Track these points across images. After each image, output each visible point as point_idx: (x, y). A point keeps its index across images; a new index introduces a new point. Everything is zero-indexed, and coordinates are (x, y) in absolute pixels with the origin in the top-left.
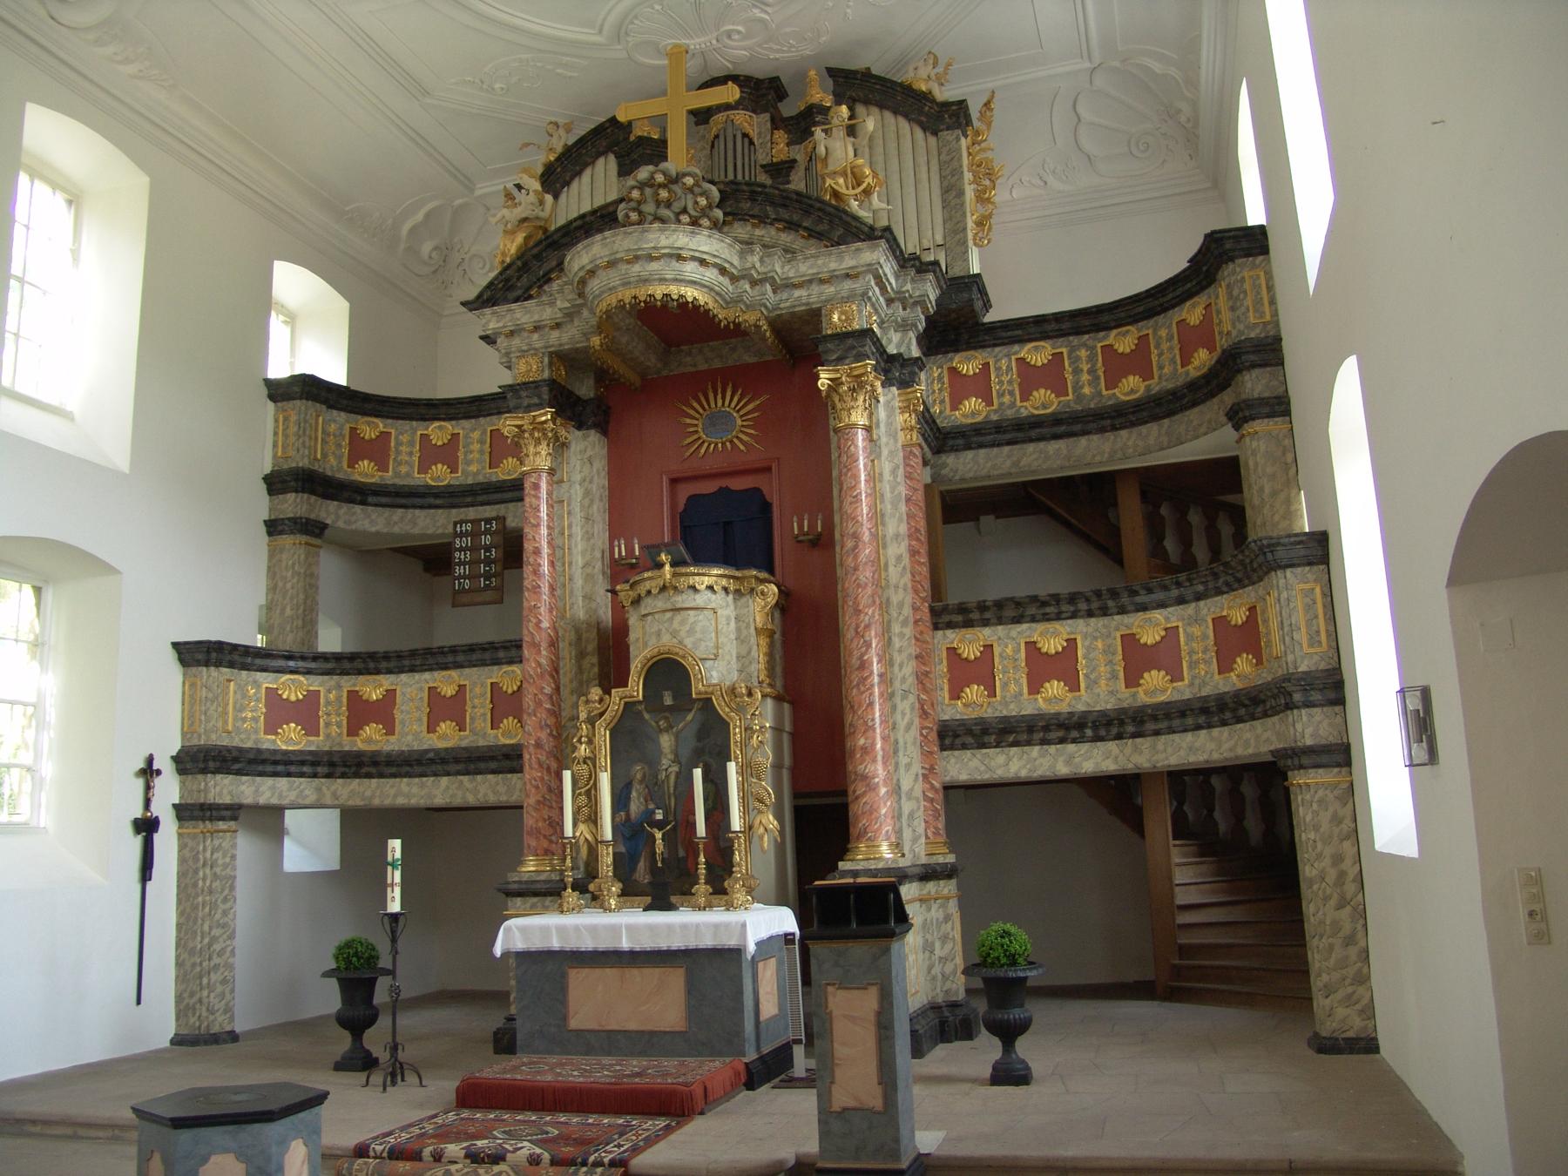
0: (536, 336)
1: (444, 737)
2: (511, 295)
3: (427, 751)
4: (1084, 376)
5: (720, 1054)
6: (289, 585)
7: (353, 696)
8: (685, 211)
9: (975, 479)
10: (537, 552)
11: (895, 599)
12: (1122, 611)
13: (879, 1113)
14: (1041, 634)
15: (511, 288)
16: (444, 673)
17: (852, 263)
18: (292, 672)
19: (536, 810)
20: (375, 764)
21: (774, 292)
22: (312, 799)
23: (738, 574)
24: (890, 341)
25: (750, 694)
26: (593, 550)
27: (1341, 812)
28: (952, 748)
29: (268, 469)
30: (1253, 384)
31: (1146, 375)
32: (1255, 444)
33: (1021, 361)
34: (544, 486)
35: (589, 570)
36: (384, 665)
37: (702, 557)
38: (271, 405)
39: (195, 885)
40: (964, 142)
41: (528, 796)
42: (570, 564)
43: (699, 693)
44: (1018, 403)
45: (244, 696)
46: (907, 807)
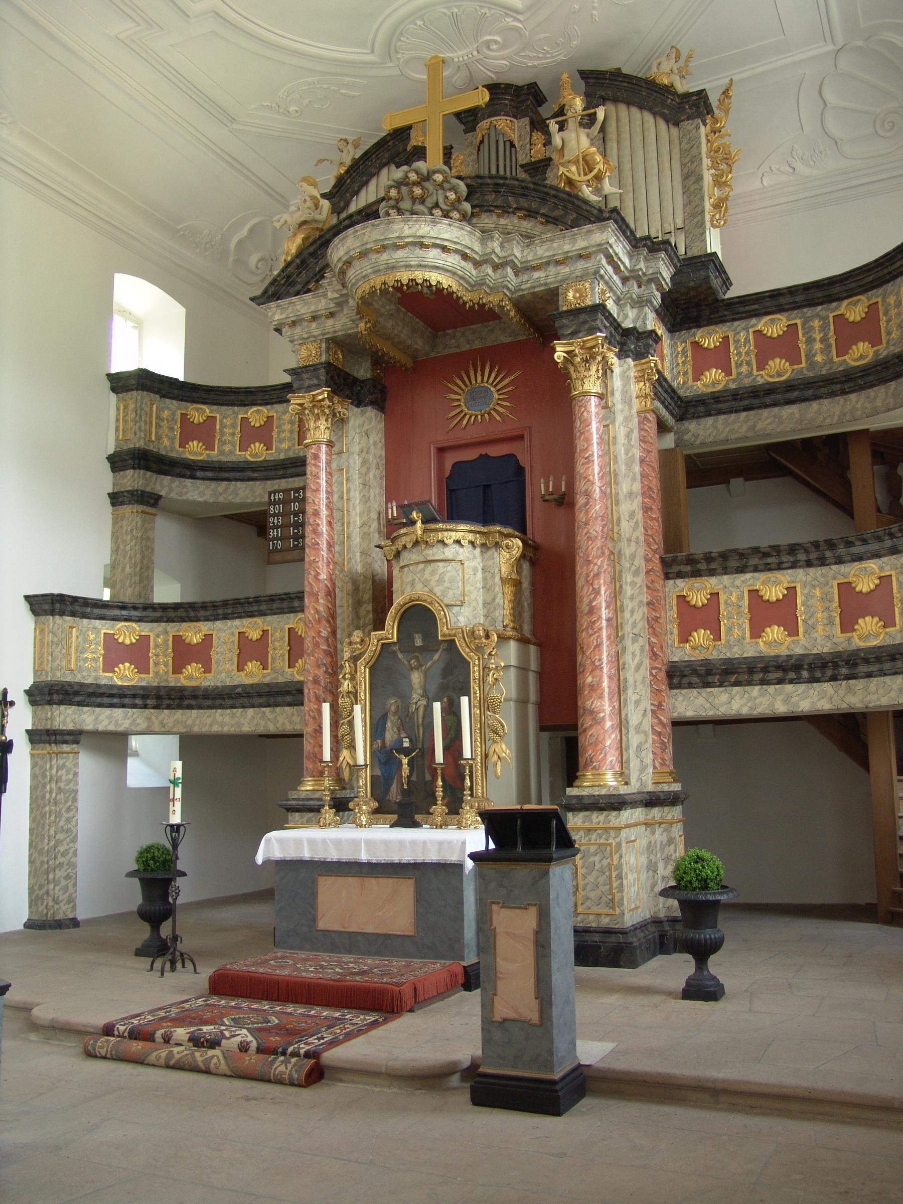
0: (314, 325)
1: (250, 674)
2: (293, 290)
3: (236, 687)
4: (817, 344)
5: (443, 957)
6: (128, 548)
7: (178, 640)
8: (437, 205)
9: (714, 443)
10: (316, 513)
11: (627, 551)
12: (839, 561)
13: (535, 1025)
14: (763, 583)
15: (292, 284)
16: (250, 620)
18: (126, 620)
19: (312, 737)
20: (195, 697)
21: (516, 275)
22: (143, 726)
23: (483, 529)
24: (626, 316)
25: (487, 636)
26: (369, 512)
28: (679, 686)
29: (111, 451)
31: (875, 341)
33: (758, 333)
34: (323, 457)
35: (366, 529)
36: (202, 613)
37: (455, 513)
38: (113, 397)
39: (43, 797)
40: (703, 130)
41: (306, 725)
42: (348, 524)
43: (444, 635)
44: (755, 372)
45: (86, 640)
46: (634, 739)
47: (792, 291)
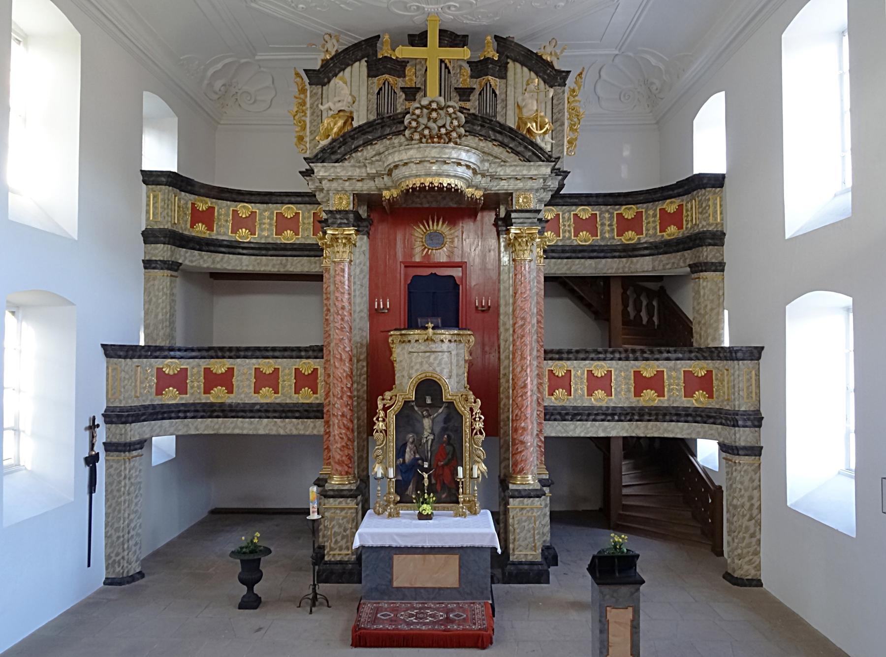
0: (347, 183)
1: (265, 396)
2: (334, 157)
6: (160, 301)
12: (636, 359)
15: (334, 153)
17: (535, 172)
18: (172, 358)
27: (754, 477)
29: (143, 229)
30: (708, 254)
32: (705, 284)
34: (347, 269)
39: (119, 491)
47: (598, 195)
